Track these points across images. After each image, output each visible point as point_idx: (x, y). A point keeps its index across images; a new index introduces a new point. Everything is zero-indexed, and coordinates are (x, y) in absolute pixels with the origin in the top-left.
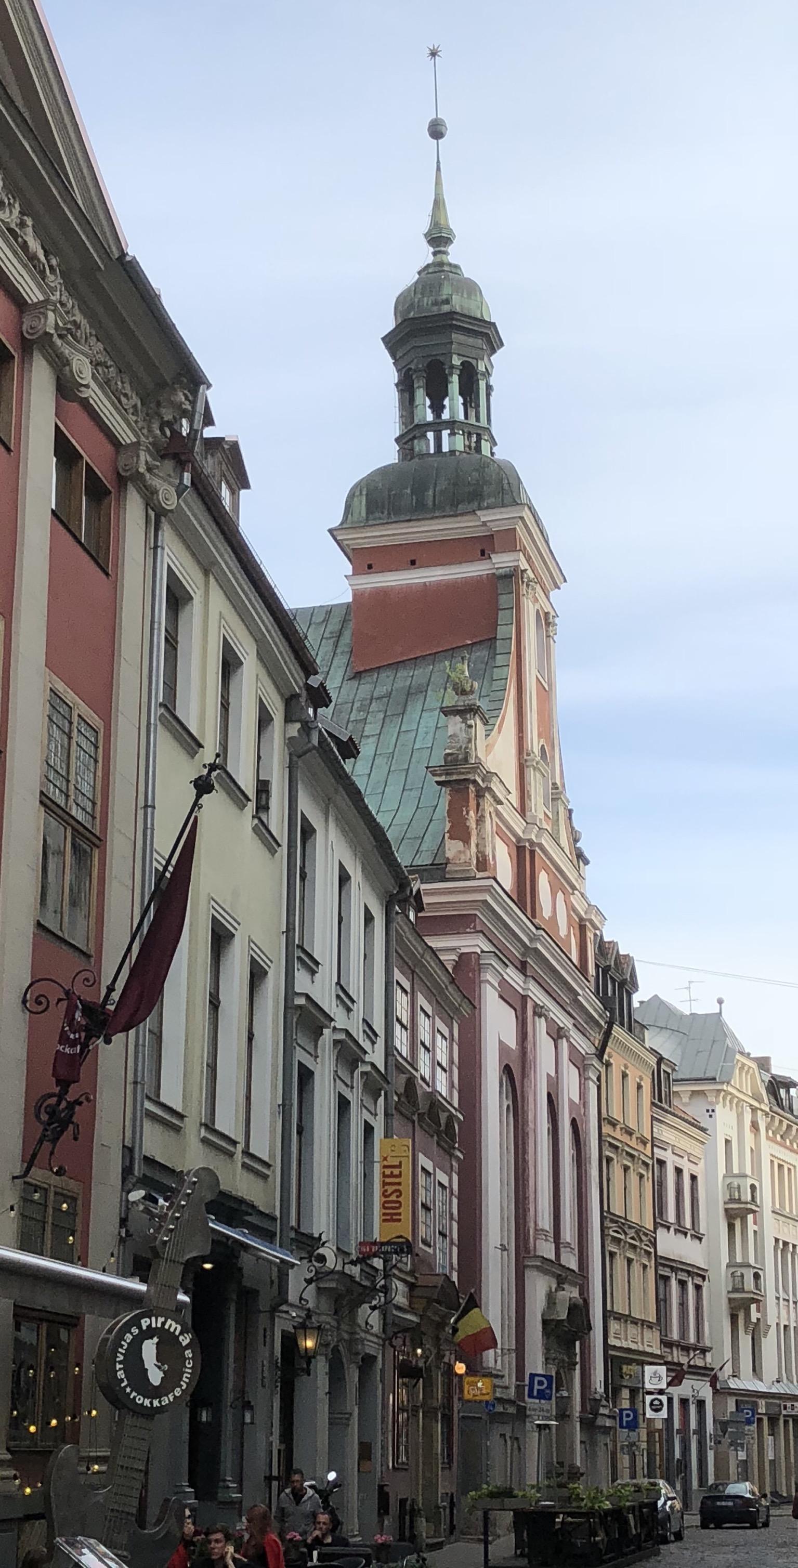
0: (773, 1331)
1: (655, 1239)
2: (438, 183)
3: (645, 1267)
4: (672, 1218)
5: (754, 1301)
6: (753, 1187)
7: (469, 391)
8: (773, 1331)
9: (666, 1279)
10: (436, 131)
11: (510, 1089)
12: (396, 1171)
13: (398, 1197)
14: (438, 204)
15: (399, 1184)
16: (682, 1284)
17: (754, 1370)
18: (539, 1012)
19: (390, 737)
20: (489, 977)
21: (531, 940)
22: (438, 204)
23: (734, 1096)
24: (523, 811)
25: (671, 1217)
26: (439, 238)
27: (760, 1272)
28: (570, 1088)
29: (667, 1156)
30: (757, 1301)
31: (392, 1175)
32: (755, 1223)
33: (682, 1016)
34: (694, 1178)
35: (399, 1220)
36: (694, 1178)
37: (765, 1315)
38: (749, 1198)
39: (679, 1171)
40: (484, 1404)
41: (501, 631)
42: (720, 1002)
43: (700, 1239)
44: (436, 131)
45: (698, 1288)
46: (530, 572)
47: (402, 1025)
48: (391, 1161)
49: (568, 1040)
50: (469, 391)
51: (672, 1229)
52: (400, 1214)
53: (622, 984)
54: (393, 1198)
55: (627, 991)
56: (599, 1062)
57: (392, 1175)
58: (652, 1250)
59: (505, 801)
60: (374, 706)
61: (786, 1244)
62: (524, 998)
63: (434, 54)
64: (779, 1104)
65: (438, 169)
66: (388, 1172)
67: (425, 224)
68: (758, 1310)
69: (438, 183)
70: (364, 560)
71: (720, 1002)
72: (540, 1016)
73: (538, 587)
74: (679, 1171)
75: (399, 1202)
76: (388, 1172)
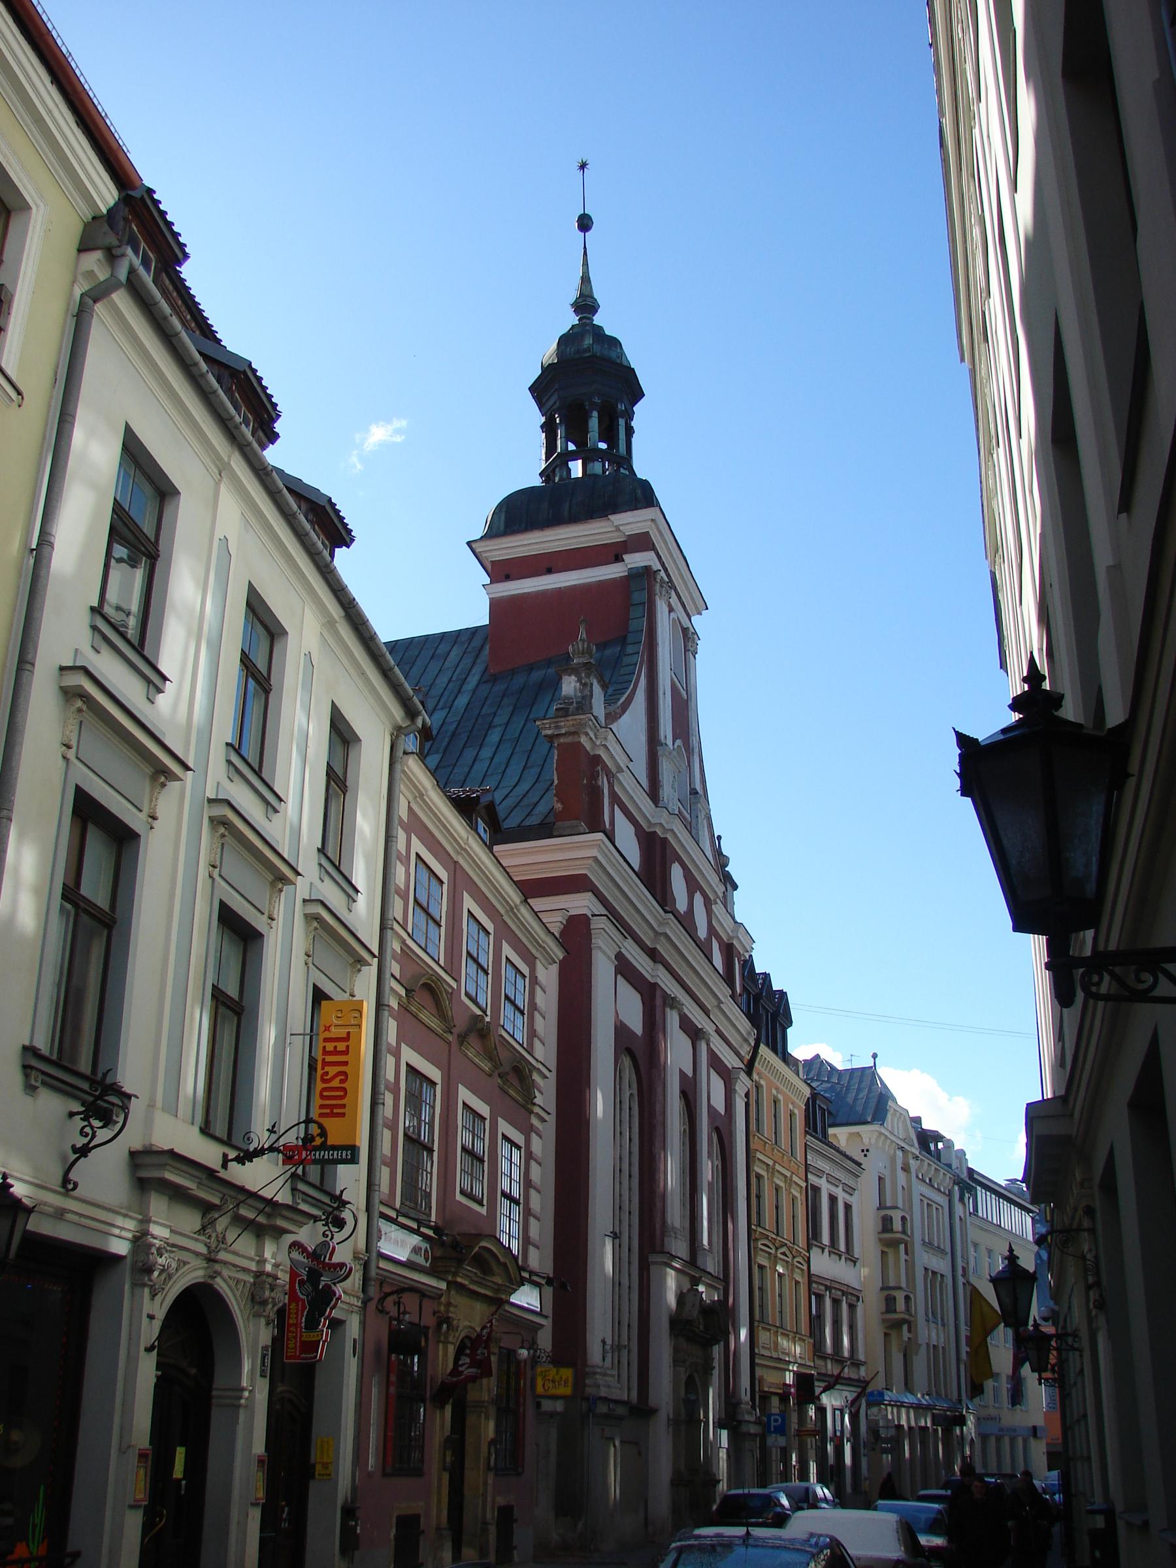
0: (923, 1350)
1: (809, 1258)
2: (585, 264)
3: (797, 1283)
4: (826, 1240)
5: (904, 1321)
6: (903, 1219)
7: (609, 434)
8: (923, 1350)
9: (820, 1297)
10: (585, 224)
11: (634, 1076)
12: (341, 1046)
13: (342, 1081)
14: (586, 280)
15: (346, 1063)
16: (836, 1302)
17: (906, 1384)
18: (672, 1002)
19: (518, 723)
20: (601, 944)
21: (660, 924)
22: (586, 280)
23: (886, 1137)
24: (654, 793)
25: (826, 1240)
26: (585, 305)
27: (912, 1296)
28: (714, 1092)
29: (823, 1183)
30: (909, 1323)
31: (335, 1052)
32: (906, 1253)
33: (841, 1073)
34: (848, 1207)
35: (343, 1115)
36: (848, 1207)
37: (916, 1337)
38: (900, 1229)
39: (833, 1199)
40: (309, 1336)
41: (633, 625)
42: (875, 1056)
43: (855, 1263)
44: (585, 224)
45: (852, 1307)
46: (662, 573)
47: (513, 1003)
48: (335, 1032)
49: (708, 1045)
50: (609, 434)
51: (826, 1251)
52: (344, 1106)
53: (775, 1016)
54: (335, 1083)
55: (781, 1024)
56: (747, 1079)
57: (335, 1052)
58: (805, 1268)
59: (625, 769)
60: (505, 701)
61: (934, 1273)
62: (655, 986)
63: (583, 166)
64: (929, 1151)
65: (585, 253)
66: (330, 1047)
67: (573, 295)
68: (909, 1331)
69: (585, 264)
70: (499, 571)
71: (875, 1056)
72: (672, 1008)
73: (673, 593)
74: (833, 1199)
75: (344, 1090)
76: (330, 1047)
